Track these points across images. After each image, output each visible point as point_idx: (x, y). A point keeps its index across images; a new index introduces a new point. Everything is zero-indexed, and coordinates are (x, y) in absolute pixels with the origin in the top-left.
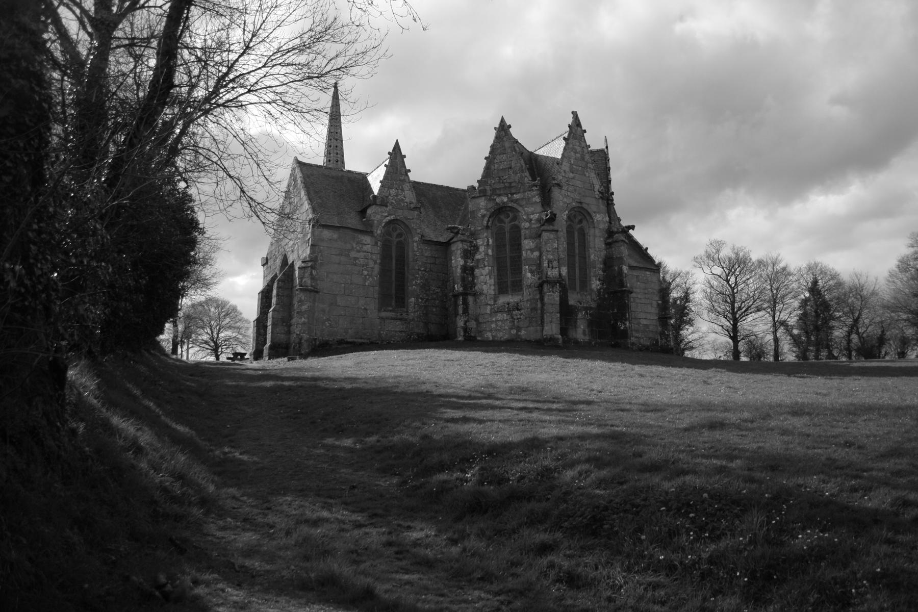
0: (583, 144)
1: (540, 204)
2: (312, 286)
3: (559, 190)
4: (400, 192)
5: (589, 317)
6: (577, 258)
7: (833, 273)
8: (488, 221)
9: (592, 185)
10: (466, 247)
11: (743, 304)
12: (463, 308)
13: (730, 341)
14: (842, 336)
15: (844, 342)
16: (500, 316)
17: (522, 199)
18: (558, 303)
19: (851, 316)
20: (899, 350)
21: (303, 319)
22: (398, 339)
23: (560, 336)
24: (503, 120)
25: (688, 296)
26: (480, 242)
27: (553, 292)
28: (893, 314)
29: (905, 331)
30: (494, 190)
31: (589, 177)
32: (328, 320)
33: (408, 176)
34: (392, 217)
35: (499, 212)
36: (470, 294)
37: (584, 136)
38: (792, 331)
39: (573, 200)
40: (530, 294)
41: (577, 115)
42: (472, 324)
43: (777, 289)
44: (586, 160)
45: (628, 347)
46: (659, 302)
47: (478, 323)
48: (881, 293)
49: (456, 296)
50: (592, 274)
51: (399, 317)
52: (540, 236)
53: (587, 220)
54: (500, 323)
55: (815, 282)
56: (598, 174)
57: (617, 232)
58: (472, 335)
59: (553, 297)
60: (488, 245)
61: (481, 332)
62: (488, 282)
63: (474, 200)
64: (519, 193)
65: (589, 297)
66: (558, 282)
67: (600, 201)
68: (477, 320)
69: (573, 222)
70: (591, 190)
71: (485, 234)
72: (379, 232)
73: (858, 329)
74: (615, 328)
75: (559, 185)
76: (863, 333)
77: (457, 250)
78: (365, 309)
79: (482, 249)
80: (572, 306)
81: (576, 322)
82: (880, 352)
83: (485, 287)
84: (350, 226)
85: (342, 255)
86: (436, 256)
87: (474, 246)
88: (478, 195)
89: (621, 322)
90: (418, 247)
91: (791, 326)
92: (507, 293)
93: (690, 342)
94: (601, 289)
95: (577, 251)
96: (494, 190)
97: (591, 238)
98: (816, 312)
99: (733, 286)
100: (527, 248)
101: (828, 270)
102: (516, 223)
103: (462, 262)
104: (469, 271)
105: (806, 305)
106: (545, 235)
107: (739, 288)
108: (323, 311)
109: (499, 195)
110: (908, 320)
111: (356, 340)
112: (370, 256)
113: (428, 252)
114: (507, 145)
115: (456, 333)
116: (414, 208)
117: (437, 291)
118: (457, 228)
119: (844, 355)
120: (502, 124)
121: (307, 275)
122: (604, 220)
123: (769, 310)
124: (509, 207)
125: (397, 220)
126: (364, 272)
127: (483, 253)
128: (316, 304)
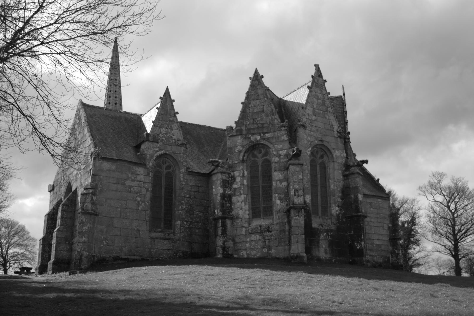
0: (324, 92)
1: (288, 142)
2: (92, 210)
4: (169, 131)
5: (330, 238)
8: (244, 156)
10: (225, 178)
11: (463, 227)
12: (222, 229)
13: (452, 259)
16: (253, 237)
18: (303, 226)
21: (84, 238)
22: (166, 257)
23: (305, 255)
24: (256, 72)
25: (415, 220)
26: (236, 173)
27: (299, 216)
30: (249, 130)
31: (329, 119)
32: (106, 239)
33: (176, 117)
34: (162, 152)
36: (228, 218)
37: (324, 85)
39: (316, 138)
40: (279, 218)
41: (319, 68)
42: (230, 244)
44: (326, 105)
45: (364, 264)
47: (235, 243)
49: (216, 220)
50: (332, 201)
51: (167, 237)
52: (287, 169)
53: (328, 156)
54: (253, 243)
56: (337, 117)
57: (353, 166)
58: (230, 253)
60: (243, 176)
61: (237, 250)
62: (243, 207)
63: (232, 138)
64: (269, 132)
65: (329, 221)
66: (303, 208)
67: (339, 139)
68: (233, 240)
70: (331, 130)
71: (241, 167)
72: (151, 164)
75: (303, 126)
77: (217, 180)
78: (138, 230)
79: (238, 180)
80: (315, 228)
81: (318, 242)
83: (241, 212)
84: (126, 159)
85: (119, 184)
86: (199, 185)
87: (232, 177)
89: (357, 242)
90: (184, 177)
93: (417, 260)
94: (339, 214)
95: (319, 182)
96: (249, 130)
97: (331, 171)
99: (453, 211)
100: (277, 178)
102: (268, 157)
103: (221, 191)
104: (227, 198)
106: (292, 168)
107: (459, 213)
109: (253, 134)
111: (129, 257)
112: (143, 185)
113: (192, 181)
114: (260, 92)
115: (216, 251)
116: (181, 144)
117: (199, 215)
118: (217, 161)
120: (256, 75)
122: (342, 155)
124: (262, 144)
125: (166, 154)
128: (96, 226)
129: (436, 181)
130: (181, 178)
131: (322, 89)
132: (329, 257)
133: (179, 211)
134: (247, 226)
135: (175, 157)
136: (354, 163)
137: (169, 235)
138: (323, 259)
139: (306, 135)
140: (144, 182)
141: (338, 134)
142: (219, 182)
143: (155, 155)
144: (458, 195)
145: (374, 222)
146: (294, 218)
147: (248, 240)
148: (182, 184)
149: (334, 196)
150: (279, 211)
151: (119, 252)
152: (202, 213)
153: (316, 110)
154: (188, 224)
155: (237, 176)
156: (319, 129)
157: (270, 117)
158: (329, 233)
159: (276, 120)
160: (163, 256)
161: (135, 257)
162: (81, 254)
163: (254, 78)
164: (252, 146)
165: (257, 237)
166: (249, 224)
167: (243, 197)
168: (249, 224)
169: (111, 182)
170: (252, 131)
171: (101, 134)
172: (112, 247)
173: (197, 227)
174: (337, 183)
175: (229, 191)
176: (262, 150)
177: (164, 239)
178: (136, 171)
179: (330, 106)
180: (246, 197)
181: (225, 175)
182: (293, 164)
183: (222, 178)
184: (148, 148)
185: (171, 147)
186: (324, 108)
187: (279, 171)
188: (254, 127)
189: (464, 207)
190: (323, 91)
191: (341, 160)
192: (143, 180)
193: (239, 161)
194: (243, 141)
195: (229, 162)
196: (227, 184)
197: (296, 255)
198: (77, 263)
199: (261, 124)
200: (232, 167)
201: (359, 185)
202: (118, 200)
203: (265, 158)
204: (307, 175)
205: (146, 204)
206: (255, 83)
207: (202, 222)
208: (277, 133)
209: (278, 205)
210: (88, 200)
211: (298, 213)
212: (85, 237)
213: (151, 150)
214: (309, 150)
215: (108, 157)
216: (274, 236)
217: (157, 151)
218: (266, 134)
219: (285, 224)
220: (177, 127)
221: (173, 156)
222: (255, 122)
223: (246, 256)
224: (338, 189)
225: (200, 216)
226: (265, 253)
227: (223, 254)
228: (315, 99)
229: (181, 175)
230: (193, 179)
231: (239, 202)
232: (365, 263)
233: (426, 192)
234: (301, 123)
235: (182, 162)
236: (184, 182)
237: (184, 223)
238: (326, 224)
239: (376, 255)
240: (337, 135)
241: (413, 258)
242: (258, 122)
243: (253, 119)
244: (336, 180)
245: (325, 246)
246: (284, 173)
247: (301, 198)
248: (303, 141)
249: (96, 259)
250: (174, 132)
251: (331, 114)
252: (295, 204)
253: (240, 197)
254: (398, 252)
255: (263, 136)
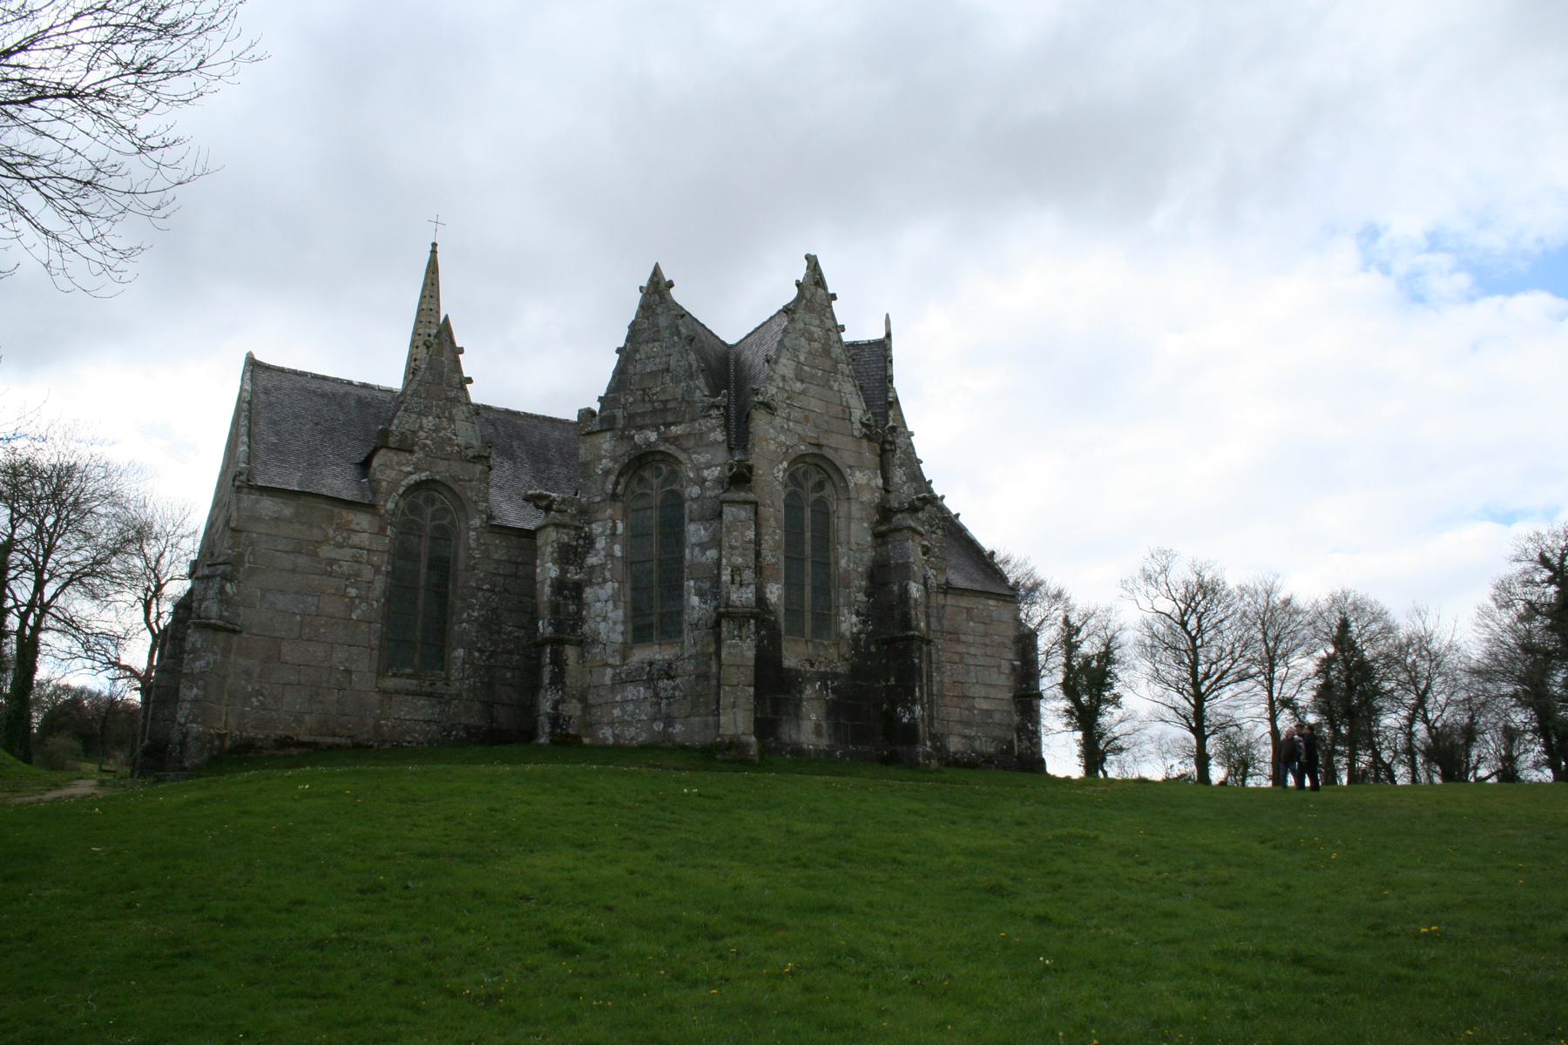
0: (829, 323)
2: (221, 617)
3: (769, 417)
4: (445, 423)
5: (831, 696)
6: (808, 567)
7: (1377, 609)
8: (617, 483)
9: (847, 408)
10: (566, 539)
11: (1214, 666)
12: (552, 671)
13: (1192, 737)
14: (1398, 725)
15: (1401, 738)
16: (631, 692)
17: (689, 434)
18: (752, 663)
19: (1412, 688)
20: (1503, 752)
21: (195, 690)
22: (421, 738)
23: (753, 739)
24: (656, 272)
25: (1112, 653)
26: (597, 528)
27: (740, 638)
28: (1489, 686)
29: (1513, 717)
30: (631, 417)
31: (839, 391)
32: (258, 693)
33: (465, 390)
34: (424, 476)
35: (640, 462)
37: (830, 307)
38: (1304, 717)
39: (802, 439)
40: (695, 643)
41: (816, 264)
42: (573, 709)
43: (1277, 639)
44: (833, 355)
45: (918, 764)
46: (1016, 663)
47: (586, 707)
48: (1464, 647)
49: (540, 646)
50: (841, 600)
51: (426, 688)
52: (720, 515)
53: (834, 484)
54: (630, 707)
55: (1344, 625)
56: (861, 388)
57: (900, 511)
58: (571, 731)
59: (741, 649)
60: (613, 534)
61: (591, 725)
62: (610, 615)
63: (589, 439)
64: (680, 423)
65: (832, 650)
66: (753, 616)
67: (865, 443)
68: (583, 699)
69: (802, 488)
70: (844, 419)
71: (609, 512)
72: (390, 506)
73: (1425, 711)
74: (890, 718)
75: (768, 407)
76: (1436, 720)
77: (546, 544)
78: (348, 672)
79: (600, 544)
80: (789, 670)
81: (798, 706)
82: (1468, 756)
83: (602, 627)
84: (324, 491)
85: (300, 553)
86: (519, 560)
88: (598, 428)
90: (478, 539)
91: (1302, 707)
92: (651, 641)
93: (1116, 738)
94: (860, 633)
95: (808, 550)
96: (631, 417)
97: (842, 523)
98: (1348, 681)
99: (1193, 633)
100: (693, 540)
101: (1366, 603)
102: (676, 487)
103: (553, 571)
104: (571, 591)
105: (1329, 668)
106: (729, 512)
107: (1206, 639)
108: (248, 673)
109: (641, 428)
110: (1515, 695)
111: (319, 739)
114: (663, 321)
116: (474, 457)
117: (516, 634)
118: (547, 497)
119: (1401, 762)
120: (655, 279)
121: (211, 593)
122: (873, 484)
123: (1262, 678)
124: (661, 452)
125: (434, 481)
126: (349, 590)
127: (603, 553)
128: (232, 658)
129: (1158, 569)
130: (471, 542)
131: (825, 315)
132: (827, 746)
133: (461, 623)
134: (618, 663)
135: (456, 487)
136: (901, 503)
137: (432, 684)
138: (809, 750)
139: (774, 428)
140: (369, 550)
141: (864, 430)
142: (549, 549)
143: (403, 483)
144: (1204, 598)
145: (975, 655)
146: (729, 642)
147: (618, 698)
148: (472, 557)
149: (848, 587)
150: (696, 625)
151: (294, 725)
152: (523, 631)
153: (806, 368)
154: (484, 658)
155: (597, 536)
156: (812, 415)
157: (683, 384)
158: (829, 683)
159: (698, 391)
160: (411, 736)
161: (337, 740)
162: (184, 731)
163: (651, 289)
164: (635, 458)
165: (638, 691)
166: (624, 658)
167: (609, 588)
168: (624, 658)
169: (280, 548)
170: (639, 419)
171: (277, 433)
172: (274, 713)
173: (508, 664)
174: (857, 555)
175: (576, 574)
176: (663, 467)
177: (419, 695)
178: (350, 522)
179: (844, 358)
180: (619, 589)
181: (566, 531)
182: (733, 502)
183: (558, 539)
184: (385, 465)
185: (446, 462)
186: (828, 364)
187: (699, 520)
188: (644, 410)
189: (1217, 623)
190: (826, 321)
191: (869, 497)
192: (366, 544)
193: (604, 495)
194: (615, 446)
195: (580, 500)
196: (570, 555)
197: (727, 741)
198: (174, 754)
199: (662, 401)
200: (586, 513)
201: (912, 560)
202: (296, 593)
203: (668, 488)
204: (774, 532)
205: (372, 605)
206: (653, 299)
207: (521, 652)
208: (700, 424)
209: (693, 608)
210: (211, 593)
211: (740, 628)
212: (197, 686)
213: (394, 469)
214: (781, 467)
215: (273, 485)
216: (681, 690)
217: (410, 473)
218: (672, 428)
219: (711, 659)
220: (467, 415)
221: (452, 486)
222: (647, 398)
223: (611, 741)
224: (860, 570)
225: (518, 637)
226: (659, 733)
227: (552, 734)
228: (803, 339)
229: (472, 533)
230: (504, 544)
231: (599, 601)
232: (920, 759)
233: (1136, 591)
234: (761, 398)
235: (475, 502)
236: (476, 552)
237: (473, 655)
238: (823, 659)
239: (979, 734)
240: (861, 432)
241: (1110, 735)
242: (655, 397)
243: (644, 390)
244: (855, 547)
245: (817, 716)
246: (713, 526)
247: (749, 591)
248: (764, 443)
249: (228, 743)
250: (457, 427)
251: (846, 379)
252: (732, 607)
253: (603, 588)
254: (1034, 728)
255: (664, 433)
